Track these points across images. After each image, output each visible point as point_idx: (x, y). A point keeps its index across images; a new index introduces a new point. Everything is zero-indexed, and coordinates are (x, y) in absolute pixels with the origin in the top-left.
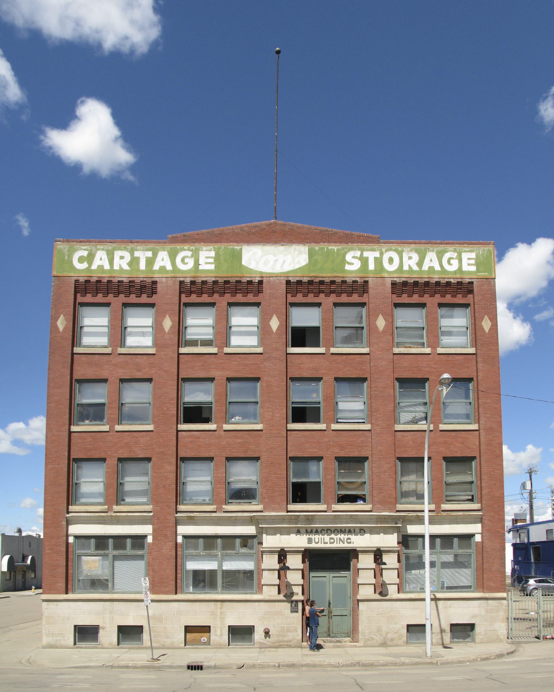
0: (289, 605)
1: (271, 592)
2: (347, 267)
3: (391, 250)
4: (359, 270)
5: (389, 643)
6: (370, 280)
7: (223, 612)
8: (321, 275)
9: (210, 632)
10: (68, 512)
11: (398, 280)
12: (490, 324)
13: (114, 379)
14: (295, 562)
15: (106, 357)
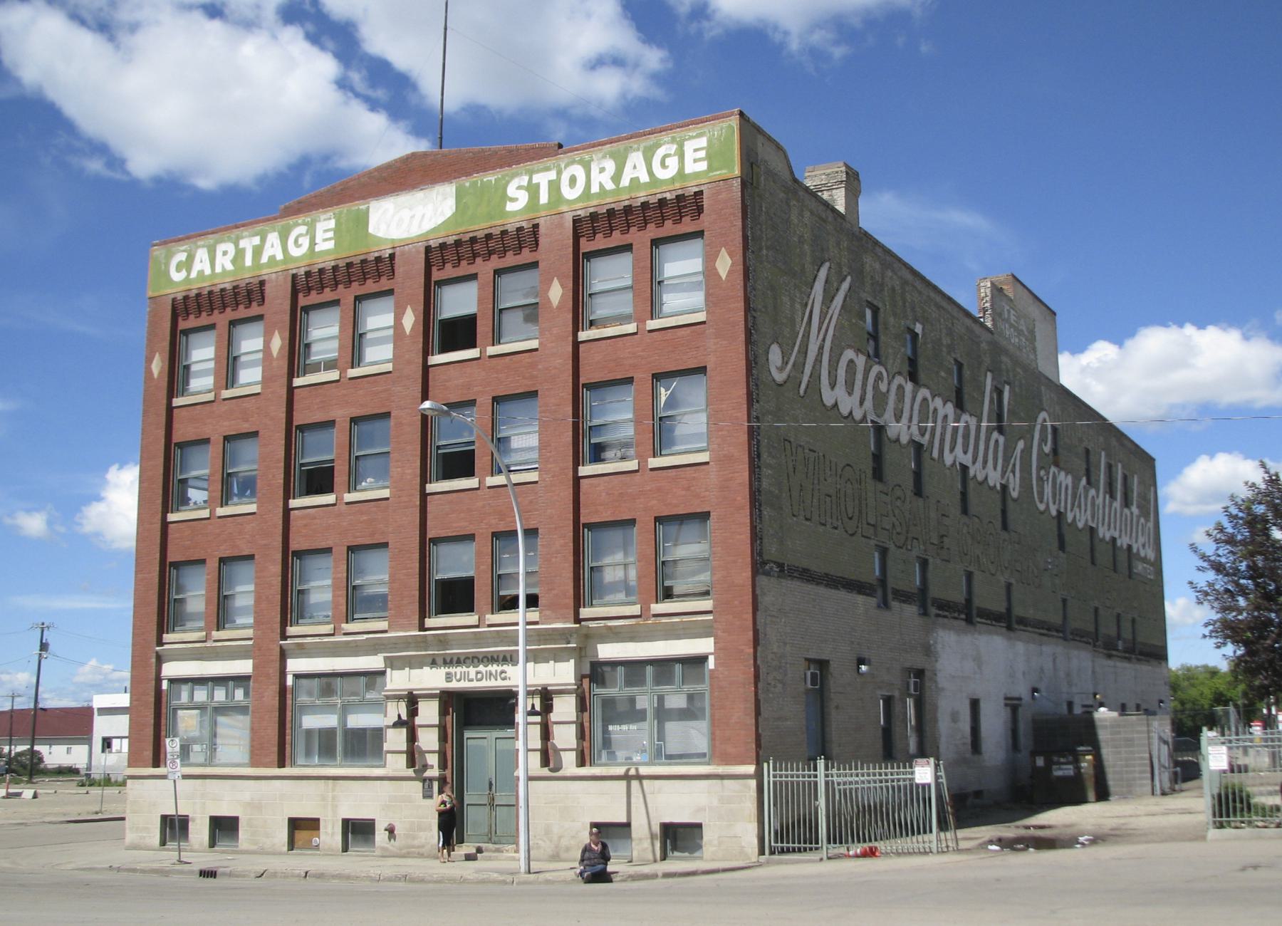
0: (419, 785)
1: (397, 764)
2: (510, 207)
3: (573, 162)
4: (527, 208)
5: (563, 855)
6: (542, 222)
7: (337, 796)
8: (472, 228)
9: (318, 828)
10: (160, 643)
11: (582, 213)
12: (730, 262)
13: (217, 439)
14: (429, 712)
15: (207, 407)
